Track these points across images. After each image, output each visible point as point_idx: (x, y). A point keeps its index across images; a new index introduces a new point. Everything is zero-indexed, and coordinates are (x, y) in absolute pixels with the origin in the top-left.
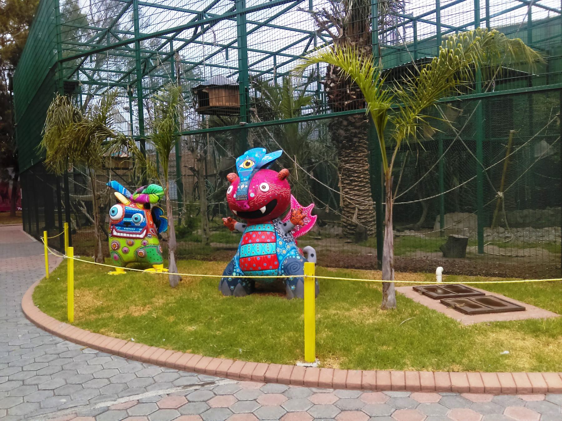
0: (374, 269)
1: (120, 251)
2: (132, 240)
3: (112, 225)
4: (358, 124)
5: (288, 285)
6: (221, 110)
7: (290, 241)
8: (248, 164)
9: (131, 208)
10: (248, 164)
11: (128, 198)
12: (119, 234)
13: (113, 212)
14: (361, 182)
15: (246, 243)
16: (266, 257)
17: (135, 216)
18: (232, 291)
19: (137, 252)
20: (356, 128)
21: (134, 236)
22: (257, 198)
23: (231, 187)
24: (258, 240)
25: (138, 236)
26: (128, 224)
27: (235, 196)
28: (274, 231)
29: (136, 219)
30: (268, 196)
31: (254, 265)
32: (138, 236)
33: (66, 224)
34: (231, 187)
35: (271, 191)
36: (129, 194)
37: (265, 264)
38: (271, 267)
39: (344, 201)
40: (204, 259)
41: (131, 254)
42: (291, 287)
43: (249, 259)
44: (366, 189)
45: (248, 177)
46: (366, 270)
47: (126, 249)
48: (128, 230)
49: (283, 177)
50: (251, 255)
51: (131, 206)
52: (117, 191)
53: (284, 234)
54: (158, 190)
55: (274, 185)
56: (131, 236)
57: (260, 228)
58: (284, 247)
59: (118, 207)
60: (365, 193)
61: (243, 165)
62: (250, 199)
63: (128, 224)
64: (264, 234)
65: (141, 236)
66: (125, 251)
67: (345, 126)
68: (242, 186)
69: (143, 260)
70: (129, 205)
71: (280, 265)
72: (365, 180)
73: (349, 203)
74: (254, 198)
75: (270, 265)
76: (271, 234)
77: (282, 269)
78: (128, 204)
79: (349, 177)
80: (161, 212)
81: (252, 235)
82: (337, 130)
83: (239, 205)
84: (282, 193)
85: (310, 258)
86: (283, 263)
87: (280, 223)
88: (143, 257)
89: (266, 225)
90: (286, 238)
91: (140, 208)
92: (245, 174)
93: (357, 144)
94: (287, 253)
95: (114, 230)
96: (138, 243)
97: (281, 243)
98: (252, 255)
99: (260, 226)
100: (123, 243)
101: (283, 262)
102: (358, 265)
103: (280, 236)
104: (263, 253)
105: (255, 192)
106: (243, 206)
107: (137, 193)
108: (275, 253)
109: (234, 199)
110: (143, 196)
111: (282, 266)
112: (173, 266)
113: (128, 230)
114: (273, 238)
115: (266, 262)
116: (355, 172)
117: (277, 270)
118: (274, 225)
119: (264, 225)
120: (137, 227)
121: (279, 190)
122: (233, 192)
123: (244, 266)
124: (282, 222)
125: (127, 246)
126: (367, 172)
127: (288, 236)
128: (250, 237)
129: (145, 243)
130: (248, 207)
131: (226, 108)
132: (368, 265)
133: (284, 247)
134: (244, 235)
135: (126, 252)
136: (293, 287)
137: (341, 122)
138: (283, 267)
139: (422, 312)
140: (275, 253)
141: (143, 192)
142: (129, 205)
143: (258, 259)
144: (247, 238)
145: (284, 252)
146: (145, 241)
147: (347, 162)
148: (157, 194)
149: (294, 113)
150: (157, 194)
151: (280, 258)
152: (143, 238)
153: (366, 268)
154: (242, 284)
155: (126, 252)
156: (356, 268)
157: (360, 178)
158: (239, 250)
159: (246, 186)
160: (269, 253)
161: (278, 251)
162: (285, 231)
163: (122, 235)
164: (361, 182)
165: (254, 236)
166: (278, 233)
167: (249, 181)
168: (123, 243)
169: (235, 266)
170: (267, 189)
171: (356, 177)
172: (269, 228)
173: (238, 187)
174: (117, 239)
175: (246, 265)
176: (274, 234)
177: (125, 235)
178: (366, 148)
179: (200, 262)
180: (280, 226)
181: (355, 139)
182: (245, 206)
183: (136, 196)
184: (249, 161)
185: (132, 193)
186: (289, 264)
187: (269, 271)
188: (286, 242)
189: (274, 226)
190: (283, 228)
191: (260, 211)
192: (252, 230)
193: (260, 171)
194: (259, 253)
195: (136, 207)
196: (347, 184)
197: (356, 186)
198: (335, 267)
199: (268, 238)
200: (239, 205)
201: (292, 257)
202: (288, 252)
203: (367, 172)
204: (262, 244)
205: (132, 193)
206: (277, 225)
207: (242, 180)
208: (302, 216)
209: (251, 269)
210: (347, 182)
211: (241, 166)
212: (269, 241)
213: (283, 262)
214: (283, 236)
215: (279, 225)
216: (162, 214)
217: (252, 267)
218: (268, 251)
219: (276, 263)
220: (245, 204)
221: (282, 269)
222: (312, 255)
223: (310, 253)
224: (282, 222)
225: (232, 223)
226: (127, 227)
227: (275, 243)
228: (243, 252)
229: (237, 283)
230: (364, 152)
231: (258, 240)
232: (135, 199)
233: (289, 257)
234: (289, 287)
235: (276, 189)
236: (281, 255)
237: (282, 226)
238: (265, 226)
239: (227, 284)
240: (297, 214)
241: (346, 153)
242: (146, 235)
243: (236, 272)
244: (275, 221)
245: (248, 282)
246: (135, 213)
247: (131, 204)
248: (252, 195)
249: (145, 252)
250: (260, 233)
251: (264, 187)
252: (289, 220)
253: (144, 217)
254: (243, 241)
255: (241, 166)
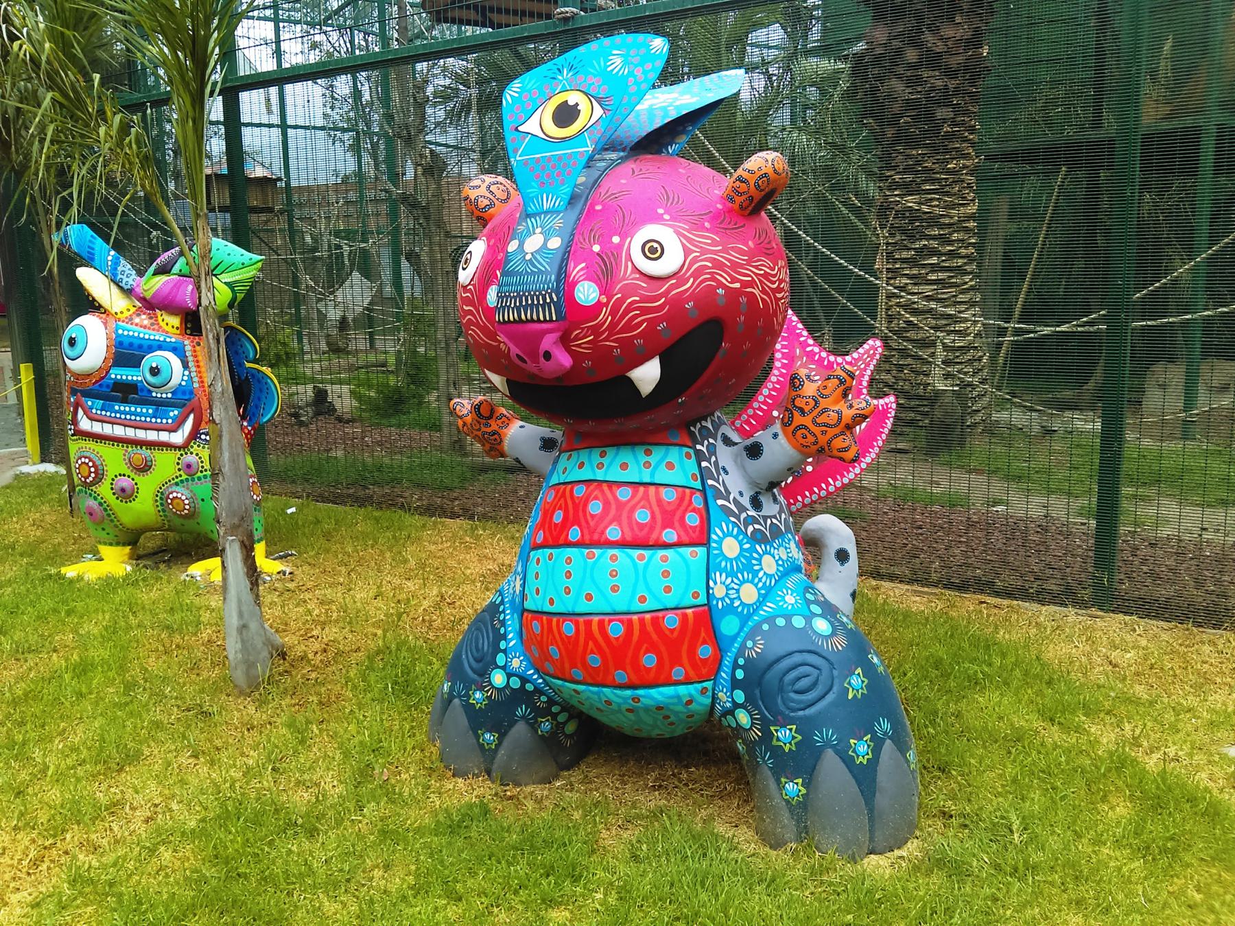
0: (1080, 604)
1: (104, 490)
2: (145, 452)
3: (74, 392)
4: (955, 61)
5: (766, 773)
6: (511, 19)
7: (776, 533)
8: (565, 115)
9: (139, 328)
10: (565, 115)
11: (128, 292)
12: (97, 428)
13: (72, 342)
14: (952, 255)
15: (555, 539)
16: (656, 622)
17: (151, 360)
18: (488, 755)
19: (163, 498)
20: (951, 73)
21: (152, 436)
22: (613, 312)
23: (478, 249)
24: (613, 533)
25: (164, 436)
26: (127, 392)
27: (492, 296)
28: (698, 485)
29: (155, 371)
30: (677, 303)
31: (594, 660)
32: (164, 436)
33: (27, 370)
34: (478, 249)
35: (696, 274)
36: (129, 276)
37: (649, 660)
38: (678, 672)
39: (890, 318)
40: (429, 511)
41: (143, 507)
42: (781, 787)
43: (569, 629)
44: (967, 278)
45: (566, 190)
46: (1042, 602)
47: (125, 482)
48: (131, 413)
49: (758, 196)
50: (579, 610)
51: (137, 320)
52: (88, 262)
53: (745, 501)
54: (231, 260)
55: (706, 239)
56: (141, 434)
57: (624, 466)
58: (746, 567)
59: (89, 322)
60: (963, 292)
61: (540, 123)
62: (573, 314)
63: (127, 392)
64: (646, 496)
65: (178, 438)
66: (123, 490)
67: (912, 66)
68: (533, 243)
69: (190, 524)
70: (130, 320)
71: (727, 662)
72: (963, 251)
73: (909, 323)
74: (598, 306)
75: (676, 661)
76: (681, 499)
77: (735, 684)
78: (127, 314)
79: (912, 238)
80: (248, 346)
81: (586, 500)
82: (880, 78)
83: (515, 350)
84: (751, 284)
85: (831, 561)
86: (740, 653)
87: (727, 441)
88: (186, 517)
89: (658, 454)
90: (755, 520)
91: (168, 329)
92: (548, 172)
93: (946, 128)
94: (763, 599)
95: (80, 412)
96: (166, 464)
97: (731, 548)
98: (583, 607)
99: (625, 455)
100: (114, 460)
101: (743, 646)
102: (1015, 582)
103: (728, 512)
104: (643, 599)
105: (605, 275)
106: (534, 355)
107: (157, 273)
108: (702, 599)
109: (489, 312)
110: (177, 286)
111: (736, 666)
112: (239, 601)
113: (131, 413)
114: (692, 520)
115: (653, 648)
116: (933, 221)
117: (709, 684)
118: (699, 454)
119: (648, 453)
120: (159, 404)
121: (735, 266)
122: (486, 276)
123: (546, 656)
124: (735, 437)
125: (128, 472)
126: (972, 224)
127: (769, 508)
128: (576, 512)
129: (189, 466)
130: (564, 359)
131: (713, 627)
132: (1052, 586)
133: (749, 568)
134: (545, 496)
135: (126, 494)
136: (793, 788)
137: (899, 52)
138: (740, 674)
139: (899, 505)
140: (702, 599)
141: (176, 269)
142: (130, 320)
143: (616, 630)
144: (558, 517)
145: (749, 594)
146: (191, 459)
147: (909, 189)
148: (227, 278)
149: (729, 49)
150: (227, 278)
151: (728, 626)
152: (185, 446)
153: (1042, 597)
154: (534, 726)
155: (126, 494)
156: (997, 594)
157: (951, 243)
158: (629, 239)
159: (555, 243)
160: (671, 600)
161: (719, 591)
162: (752, 483)
163: (107, 429)
164: (952, 255)
165: (595, 507)
166: (719, 494)
167: (573, 214)
168: (114, 460)
169: (504, 637)
170: (670, 263)
171: (934, 238)
172: (670, 466)
173: (513, 246)
174: (91, 445)
175: (554, 651)
176: (698, 501)
177: (119, 431)
178: (973, 144)
179: (417, 520)
180: (725, 456)
181: (942, 113)
182: (547, 356)
183: (153, 284)
184: (573, 98)
185: (141, 273)
186: (778, 660)
187: (669, 690)
188: (759, 538)
189: (699, 454)
190: (743, 468)
191: (630, 382)
192: (586, 474)
193: (631, 165)
194: (620, 602)
195: (155, 326)
196: (904, 261)
197: (934, 268)
198: (911, 582)
199: (668, 524)
200: (515, 350)
201: (788, 618)
202: (766, 594)
203: (972, 224)
204: (635, 553)
205: (141, 273)
206: (712, 450)
207: (531, 209)
208: (848, 414)
209: (578, 673)
210: (905, 254)
211: (531, 126)
212: (670, 535)
213: (743, 646)
214: (742, 509)
215: (721, 448)
216: (251, 355)
217: (585, 666)
218: (668, 589)
219: (705, 651)
220: (548, 342)
221: (735, 684)
222: (842, 556)
223: (833, 545)
224: (735, 437)
225: (494, 427)
226: (124, 401)
227: (701, 551)
228: (539, 583)
229: (513, 723)
230: (966, 156)
231: (613, 533)
232: (148, 295)
233: (770, 620)
234: (772, 785)
235: (718, 265)
236: (730, 609)
237: (736, 457)
238: (653, 459)
239: (464, 721)
240: (824, 403)
241: (909, 157)
242: (194, 435)
243: (504, 668)
244: (704, 430)
245: (562, 718)
246: (151, 349)
247: (138, 312)
248: (587, 293)
249: (193, 498)
250: (624, 494)
251: (654, 250)
252: (777, 428)
253: (185, 365)
254: (541, 526)
255: (531, 126)
